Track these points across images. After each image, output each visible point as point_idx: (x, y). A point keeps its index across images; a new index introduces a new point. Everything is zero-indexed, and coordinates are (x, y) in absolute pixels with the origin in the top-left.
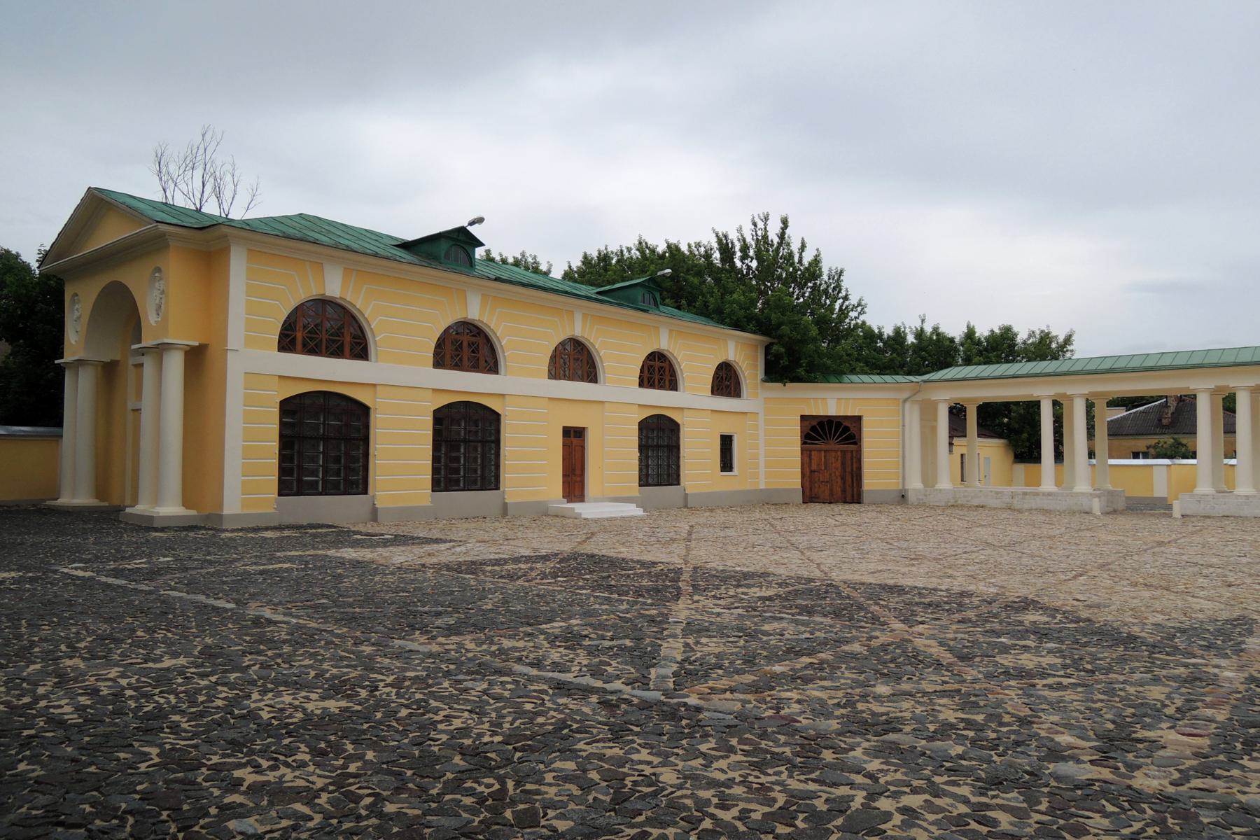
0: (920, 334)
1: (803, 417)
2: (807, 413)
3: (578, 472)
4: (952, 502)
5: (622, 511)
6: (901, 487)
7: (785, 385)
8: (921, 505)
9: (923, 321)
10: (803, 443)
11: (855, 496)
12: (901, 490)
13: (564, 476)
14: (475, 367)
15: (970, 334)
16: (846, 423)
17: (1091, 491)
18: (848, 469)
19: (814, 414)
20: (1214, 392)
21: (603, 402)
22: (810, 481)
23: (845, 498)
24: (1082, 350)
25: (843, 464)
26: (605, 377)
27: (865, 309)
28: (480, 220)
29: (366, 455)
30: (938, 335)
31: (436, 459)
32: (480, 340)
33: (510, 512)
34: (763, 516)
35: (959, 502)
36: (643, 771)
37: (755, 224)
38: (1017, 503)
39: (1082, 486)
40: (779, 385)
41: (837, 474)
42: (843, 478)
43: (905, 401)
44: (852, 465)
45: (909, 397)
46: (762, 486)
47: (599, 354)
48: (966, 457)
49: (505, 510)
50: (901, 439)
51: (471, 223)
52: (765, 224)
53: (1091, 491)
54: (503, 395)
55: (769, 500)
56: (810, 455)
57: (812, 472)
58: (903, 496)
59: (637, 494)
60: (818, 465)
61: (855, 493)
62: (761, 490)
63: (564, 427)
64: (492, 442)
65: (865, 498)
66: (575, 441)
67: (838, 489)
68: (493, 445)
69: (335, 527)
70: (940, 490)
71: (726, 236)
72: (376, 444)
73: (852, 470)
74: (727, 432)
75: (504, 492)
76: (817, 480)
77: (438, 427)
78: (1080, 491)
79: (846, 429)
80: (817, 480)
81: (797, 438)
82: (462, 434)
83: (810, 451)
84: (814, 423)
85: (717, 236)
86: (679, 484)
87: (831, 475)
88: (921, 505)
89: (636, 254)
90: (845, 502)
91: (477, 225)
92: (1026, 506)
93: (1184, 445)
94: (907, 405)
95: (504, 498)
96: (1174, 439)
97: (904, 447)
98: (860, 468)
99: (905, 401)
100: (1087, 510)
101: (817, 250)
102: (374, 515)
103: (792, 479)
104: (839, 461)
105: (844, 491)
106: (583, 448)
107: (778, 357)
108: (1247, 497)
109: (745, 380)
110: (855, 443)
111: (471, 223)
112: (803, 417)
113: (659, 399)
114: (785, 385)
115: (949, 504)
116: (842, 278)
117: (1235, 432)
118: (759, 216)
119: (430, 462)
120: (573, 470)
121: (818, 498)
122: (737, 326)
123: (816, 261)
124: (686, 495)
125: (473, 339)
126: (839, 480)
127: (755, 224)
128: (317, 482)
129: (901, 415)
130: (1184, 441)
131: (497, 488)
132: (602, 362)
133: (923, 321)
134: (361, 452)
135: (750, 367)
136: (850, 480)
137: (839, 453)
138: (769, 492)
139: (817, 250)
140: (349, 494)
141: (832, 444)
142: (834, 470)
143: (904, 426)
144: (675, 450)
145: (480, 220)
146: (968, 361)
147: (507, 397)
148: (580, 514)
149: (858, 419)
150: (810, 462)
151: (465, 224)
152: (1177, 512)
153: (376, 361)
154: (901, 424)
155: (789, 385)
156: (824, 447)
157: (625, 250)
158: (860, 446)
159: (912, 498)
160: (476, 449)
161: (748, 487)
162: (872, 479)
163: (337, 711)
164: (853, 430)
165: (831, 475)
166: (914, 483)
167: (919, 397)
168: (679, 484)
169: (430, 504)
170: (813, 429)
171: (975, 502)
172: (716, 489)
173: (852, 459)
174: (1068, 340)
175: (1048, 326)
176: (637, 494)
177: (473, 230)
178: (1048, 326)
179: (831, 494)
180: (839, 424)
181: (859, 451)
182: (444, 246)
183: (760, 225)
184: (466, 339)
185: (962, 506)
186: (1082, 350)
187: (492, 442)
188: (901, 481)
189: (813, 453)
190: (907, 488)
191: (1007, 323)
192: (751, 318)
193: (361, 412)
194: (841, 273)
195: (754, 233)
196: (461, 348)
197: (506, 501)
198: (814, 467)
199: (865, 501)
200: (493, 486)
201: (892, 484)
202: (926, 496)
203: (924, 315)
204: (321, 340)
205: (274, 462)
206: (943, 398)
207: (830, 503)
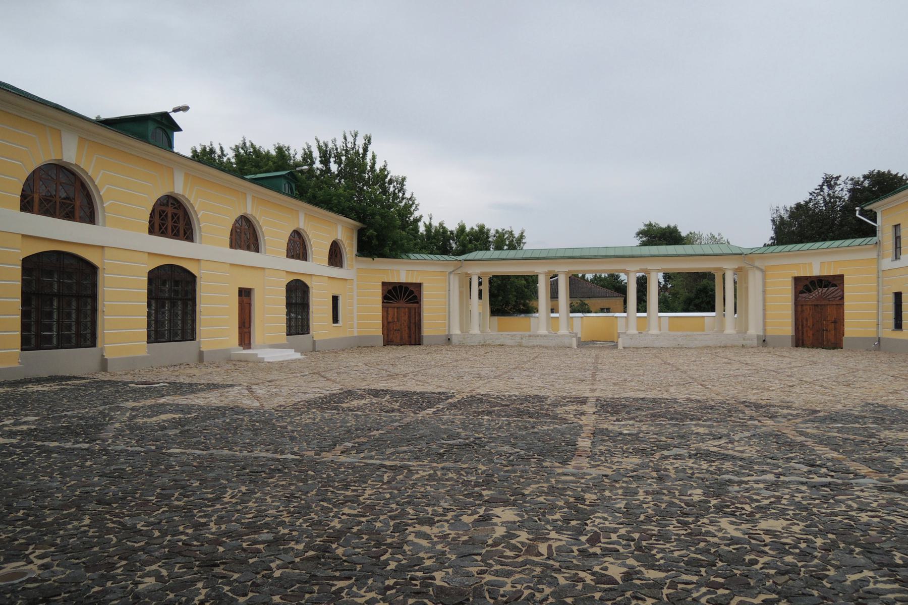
0: (429, 227)
1: (384, 284)
2: (386, 281)
3: (247, 325)
4: (482, 342)
5: (288, 355)
6: (447, 333)
7: (373, 259)
8: (461, 346)
9: (431, 218)
10: (383, 302)
11: (417, 340)
12: (448, 335)
13: (239, 327)
14: (175, 235)
15: (462, 229)
16: (411, 288)
17: (568, 333)
18: (413, 321)
19: (391, 281)
20: (546, 274)
21: (263, 269)
22: (387, 329)
23: (410, 342)
24: (531, 244)
25: (409, 317)
26: (265, 248)
27: (418, 207)
28: (185, 109)
29: (94, 311)
30: (444, 228)
31: (25, 314)
32: (181, 214)
33: (206, 358)
34: (465, 356)
35: (487, 343)
36: (736, 529)
37: (345, 138)
38: (524, 342)
39: (563, 331)
40: (370, 259)
41: (405, 324)
42: (409, 328)
43: (450, 273)
44: (415, 318)
45: (453, 271)
46: (356, 334)
47: (261, 229)
48: (891, 322)
49: (201, 356)
50: (447, 300)
51: (176, 110)
52: (355, 139)
53: (568, 333)
54: (199, 260)
55: (360, 345)
56: (387, 311)
57: (388, 323)
58: (449, 339)
59: (285, 342)
60: (392, 318)
61: (417, 337)
62: (356, 336)
63: (239, 288)
64: (189, 300)
65: (425, 341)
66: (245, 299)
67: (405, 335)
68: (89, 300)
69: (84, 378)
70: (475, 335)
71: (326, 145)
72: (104, 301)
73: (415, 323)
74: (336, 293)
75: (199, 342)
76: (392, 328)
77: (493, 299)
78: (561, 334)
79: (412, 292)
80: (392, 328)
81: (380, 298)
82: (56, 286)
83: (388, 308)
84: (390, 288)
85: (318, 142)
86: (308, 333)
87: (401, 325)
88: (461, 346)
89: (273, 153)
90: (411, 345)
91: (181, 112)
92: (531, 344)
93: (586, 305)
94: (452, 276)
95: (200, 348)
96: (581, 301)
97: (449, 305)
98: (420, 320)
99: (450, 273)
100: (568, 345)
101: (385, 162)
102: (104, 364)
103: (376, 328)
104: (407, 315)
105: (410, 337)
106: (250, 304)
107: (370, 238)
108: (657, 336)
109: (346, 255)
110: (417, 303)
111: (176, 110)
112: (384, 284)
113: (297, 267)
114: (373, 259)
115: (481, 344)
116: (405, 183)
117: (558, 298)
118: (351, 133)
119: (19, 317)
120: (244, 323)
121: (393, 342)
122: (343, 212)
123: (383, 170)
124: (314, 342)
125: (175, 211)
126: (406, 328)
127: (345, 138)
128: (51, 336)
129: (447, 282)
130: (586, 302)
131: (194, 339)
132: (264, 237)
133: (431, 218)
134: (74, 308)
135: (349, 248)
136: (414, 329)
137: (406, 309)
138: (360, 338)
139: (385, 162)
140: (62, 348)
141: (402, 304)
142: (403, 321)
143: (449, 290)
144: (190, 303)
145: (185, 109)
146: (499, 247)
147: (202, 262)
148: (263, 358)
149: (419, 286)
150: (387, 316)
151: (168, 109)
152: (620, 346)
153: (104, 225)
154: (447, 289)
155: (376, 259)
156: (396, 305)
157: (316, 154)
158: (420, 305)
159: (454, 340)
160: (69, 305)
161: (348, 335)
162: (430, 326)
163: (272, 538)
164: (416, 293)
165: (401, 325)
166: (456, 331)
167: (459, 271)
168: (308, 333)
169: (146, 354)
170: (389, 292)
171: (498, 342)
172: (332, 337)
173: (415, 314)
174: (522, 236)
175: (511, 227)
176: (285, 342)
177: (177, 117)
178: (511, 227)
179: (401, 339)
180: (407, 289)
181: (420, 308)
182: (151, 127)
183: (350, 139)
184: (170, 211)
185: (489, 345)
186: (531, 244)
187: (189, 300)
188: (447, 328)
189: (389, 309)
190: (451, 333)
191: (481, 222)
192: (352, 209)
193: (88, 271)
194: (404, 179)
195: (344, 145)
196: (172, 216)
197: (202, 350)
198: (390, 320)
199: (424, 343)
200: (190, 338)
201: (441, 331)
202: (464, 339)
203: (431, 214)
204: (55, 202)
205: (16, 318)
206: (475, 271)
207: (401, 345)
